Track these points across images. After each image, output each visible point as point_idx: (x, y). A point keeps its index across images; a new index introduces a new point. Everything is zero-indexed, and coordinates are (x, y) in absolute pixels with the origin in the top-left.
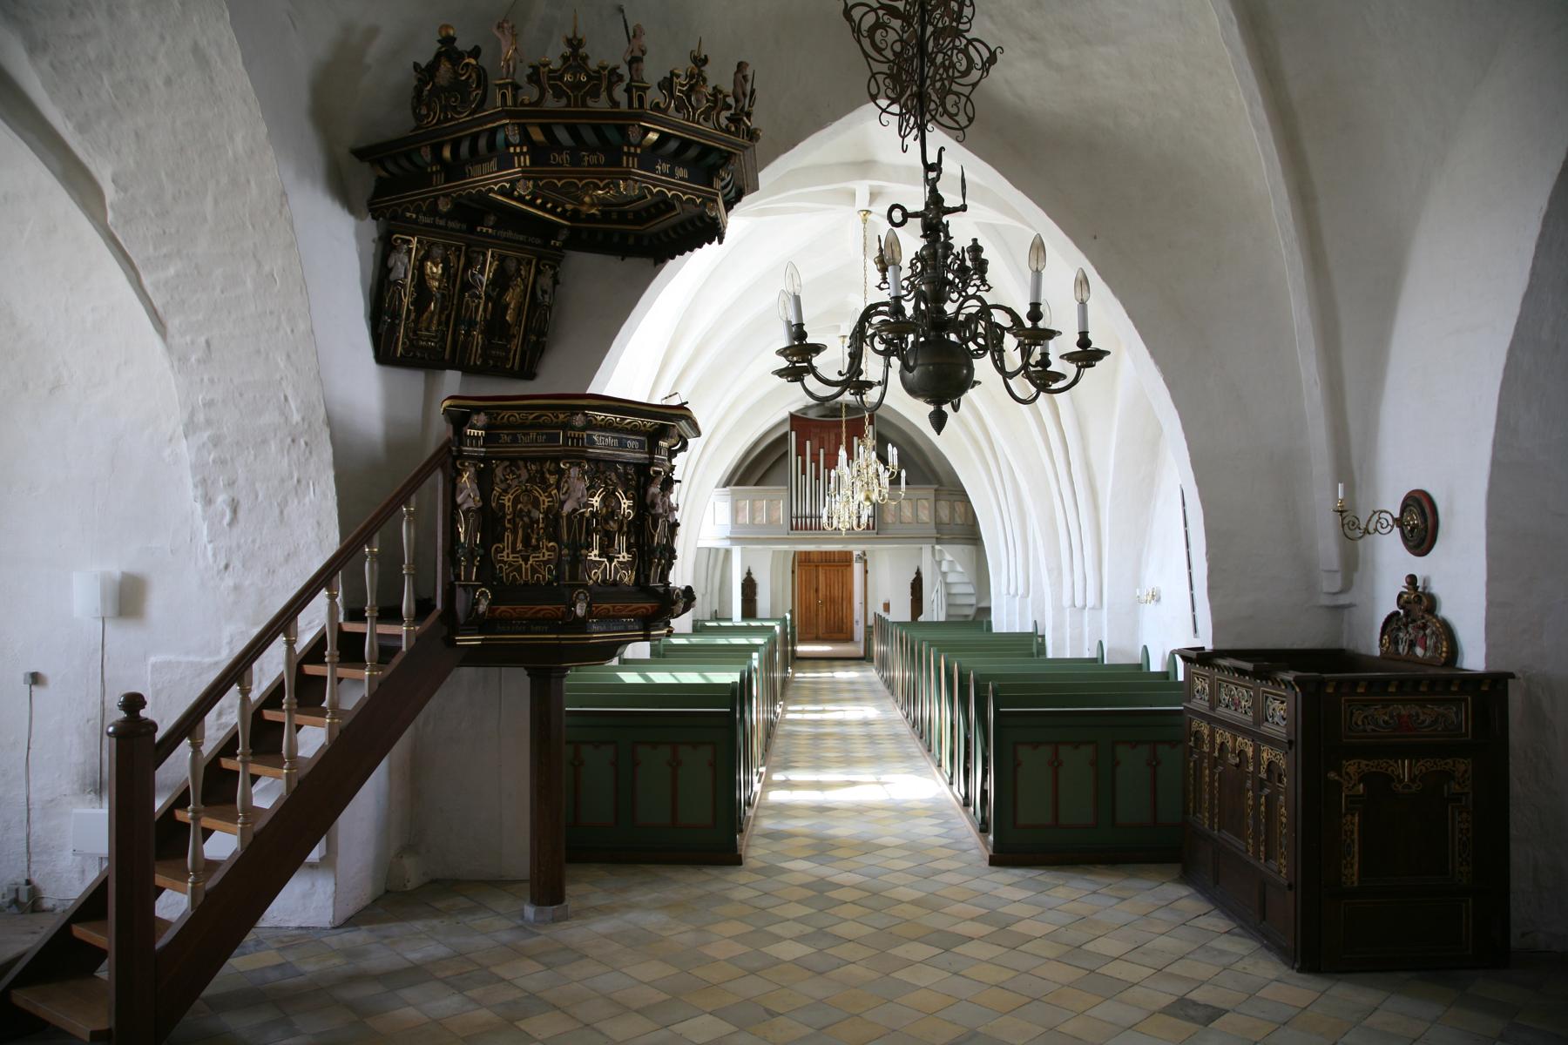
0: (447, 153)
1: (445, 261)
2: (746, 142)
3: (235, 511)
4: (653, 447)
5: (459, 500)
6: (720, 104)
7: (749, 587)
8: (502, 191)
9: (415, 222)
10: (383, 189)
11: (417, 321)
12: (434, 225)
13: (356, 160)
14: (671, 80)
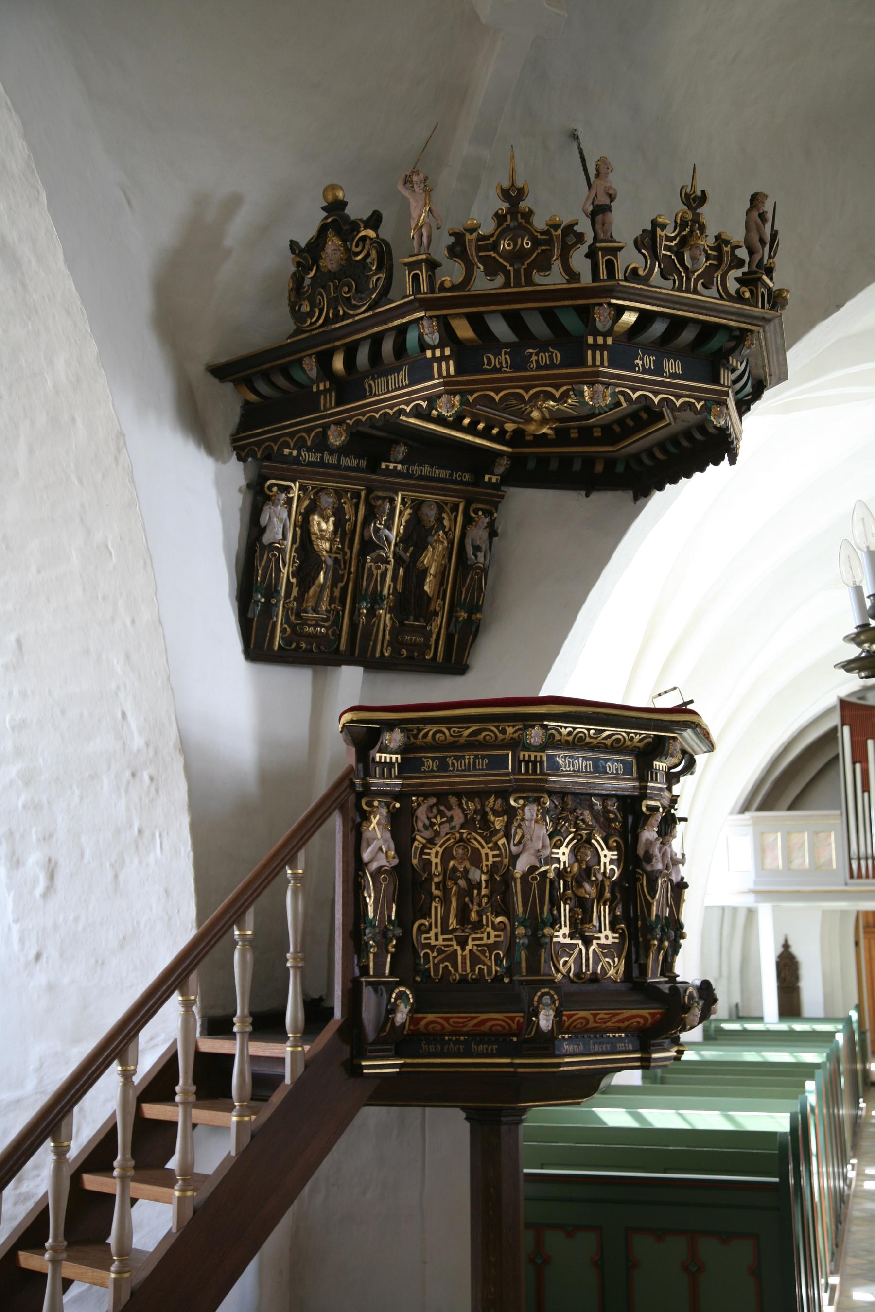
0: (338, 364)
1: (338, 513)
2: (767, 312)
3: (51, 876)
4: (645, 771)
5: (366, 856)
6: (726, 261)
7: (788, 968)
8: (417, 413)
9: (296, 461)
10: (251, 418)
11: (301, 599)
12: (322, 464)
13: (216, 381)
14: (653, 233)
